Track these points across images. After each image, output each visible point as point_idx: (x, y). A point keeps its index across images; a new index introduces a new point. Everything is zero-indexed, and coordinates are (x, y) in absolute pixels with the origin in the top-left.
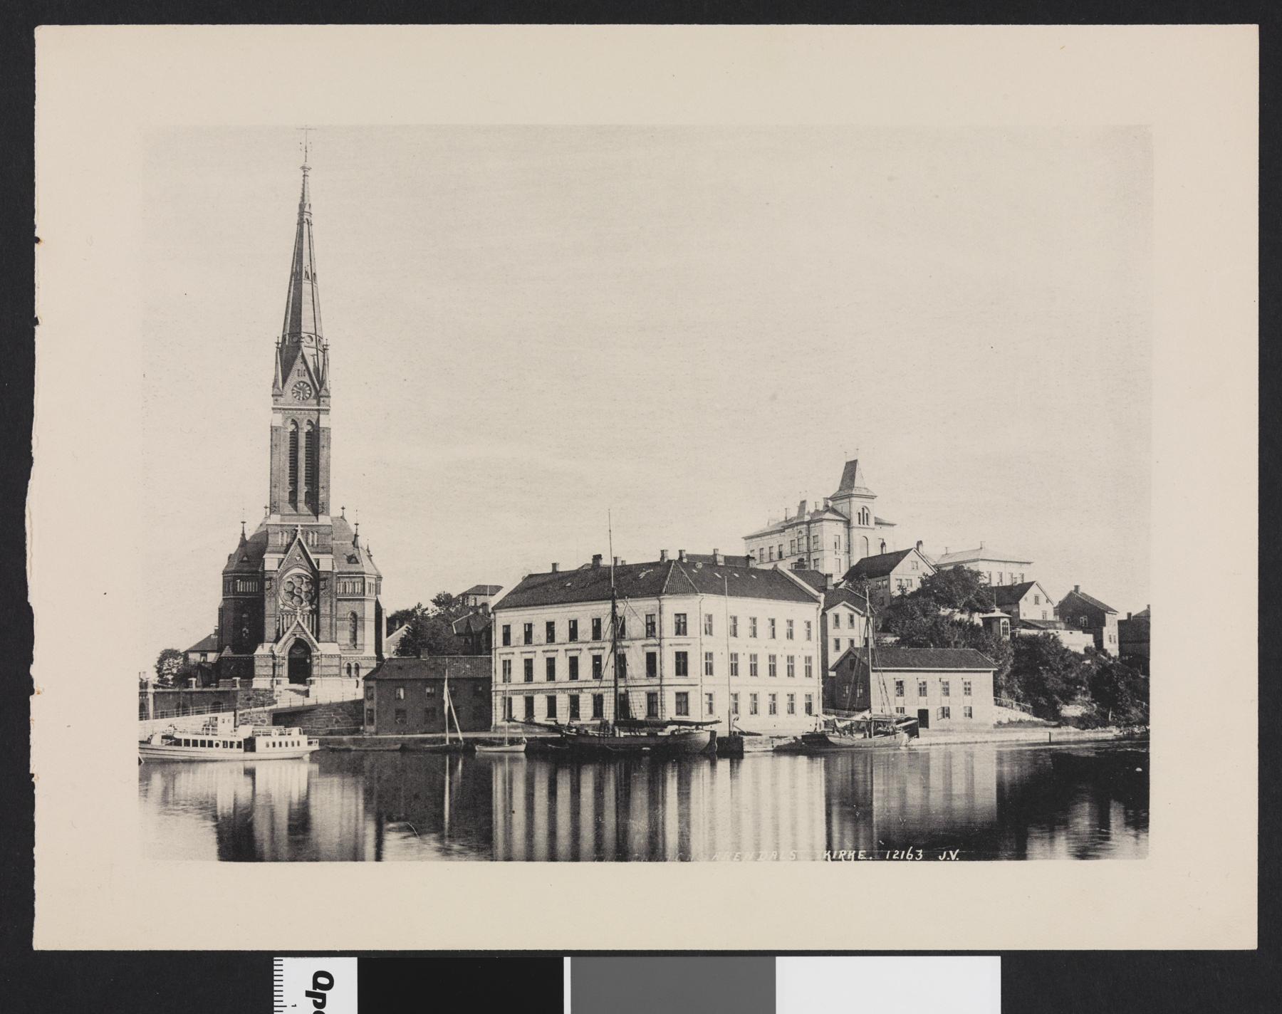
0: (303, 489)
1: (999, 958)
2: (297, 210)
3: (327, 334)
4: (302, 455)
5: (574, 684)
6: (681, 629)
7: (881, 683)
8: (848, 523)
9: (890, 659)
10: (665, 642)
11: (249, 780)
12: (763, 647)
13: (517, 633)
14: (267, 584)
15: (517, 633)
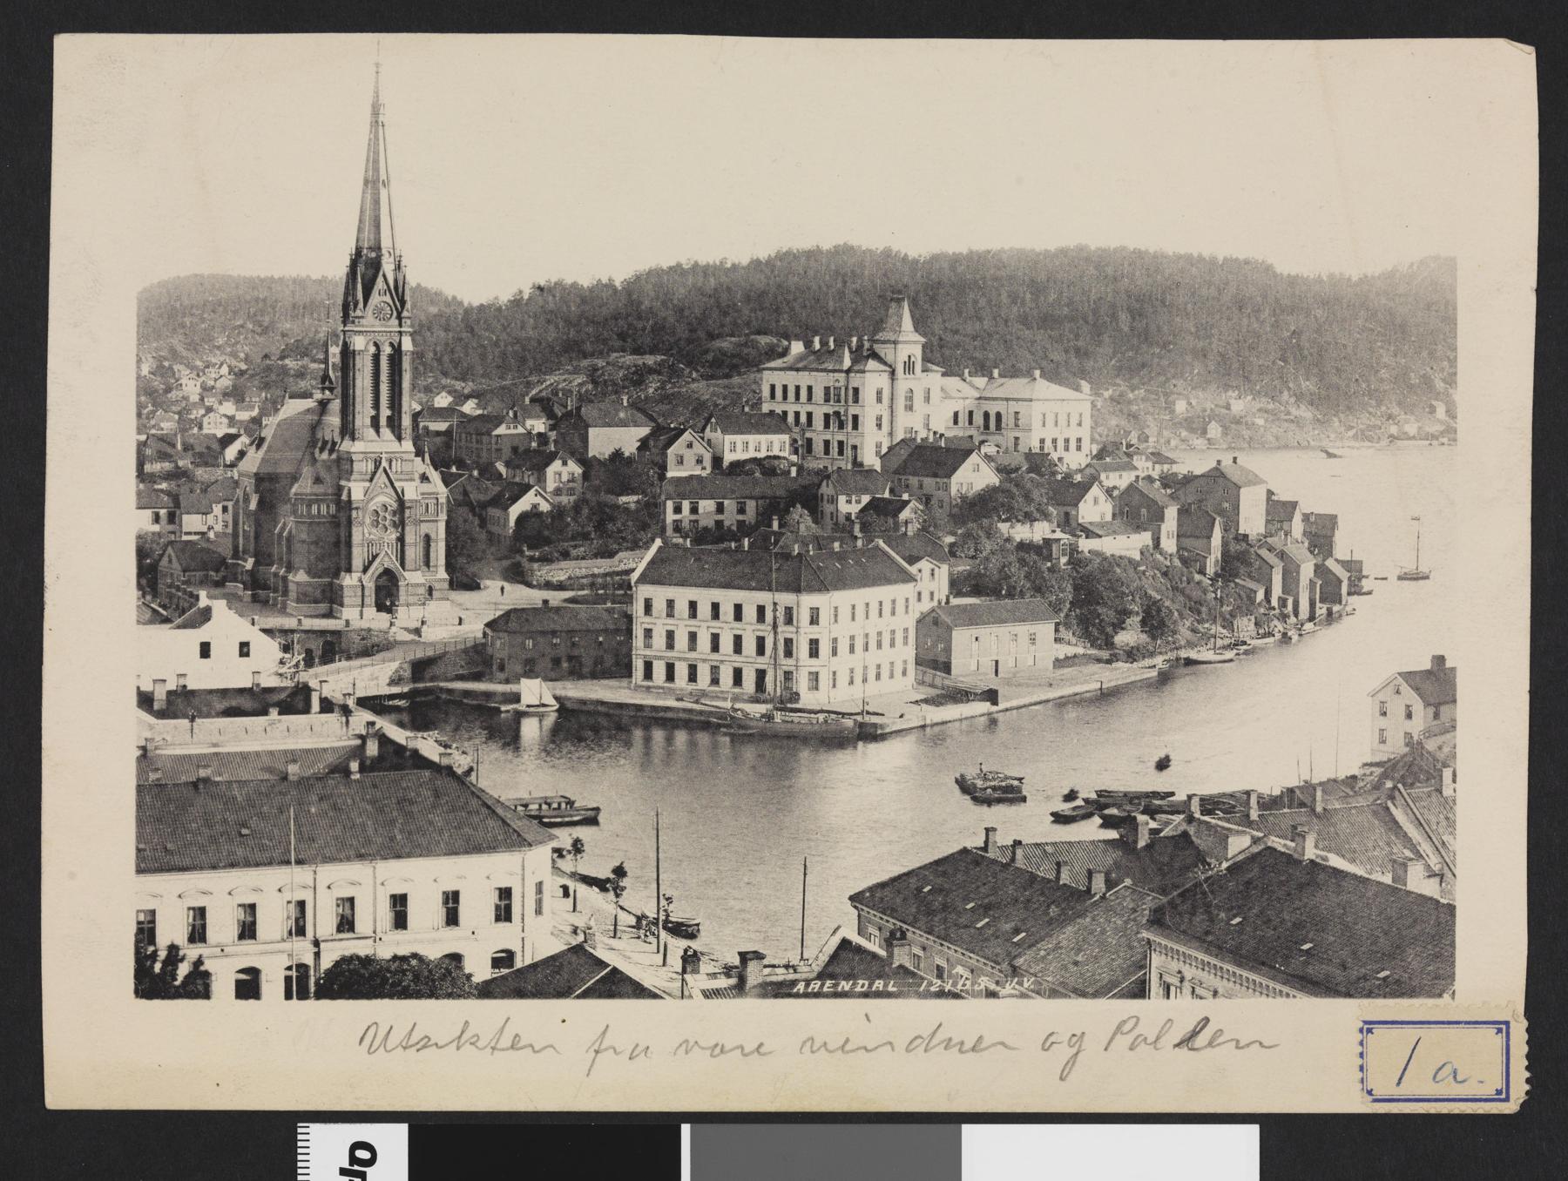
0: (385, 412)
1: (1254, 1130)
2: (368, 110)
3: (403, 248)
4: (384, 377)
5: (715, 656)
6: (814, 620)
7: (961, 638)
8: (893, 373)
9: (971, 618)
10: (802, 631)
11: (1379, 1031)
12: (874, 625)
13: (659, 606)
14: (354, 514)
15: (659, 606)
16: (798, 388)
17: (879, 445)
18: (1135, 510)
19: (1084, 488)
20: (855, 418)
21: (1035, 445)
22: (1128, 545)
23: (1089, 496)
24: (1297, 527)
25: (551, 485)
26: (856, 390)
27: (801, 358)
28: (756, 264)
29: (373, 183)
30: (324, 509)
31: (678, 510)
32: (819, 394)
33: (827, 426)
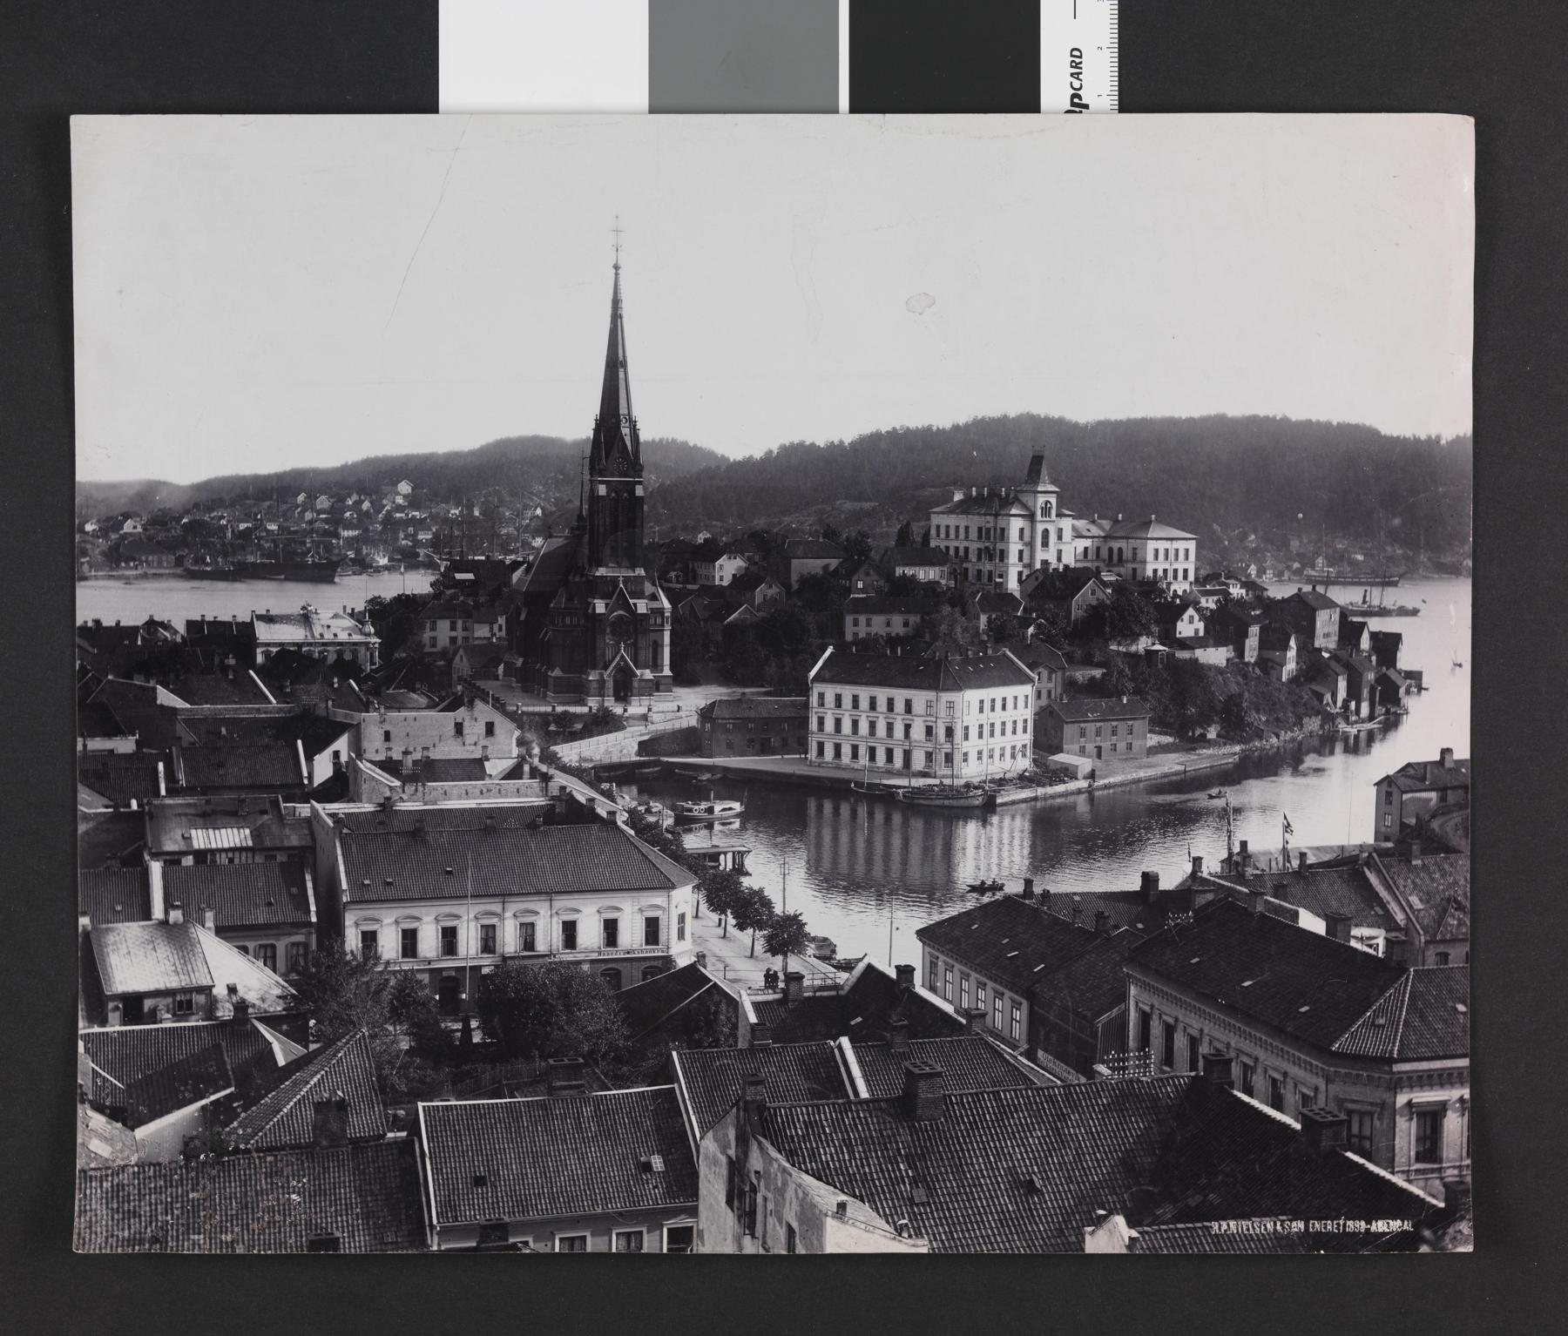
2: (609, 305)
13: (830, 699)
15: (830, 699)
16: (957, 527)
17: (1020, 574)
18: (1225, 625)
19: (1183, 608)
20: (1002, 552)
21: (1149, 573)
22: (1216, 656)
23: (1186, 617)
24: (1365, 643)
25: (758, 599)
26: (1003, 530)
27: (961, 502)
28: (956, 428)
29: (615, 365)
30: (575, 620)
31: (856, 623)
32: (973, 534)
33: (979, 559)
